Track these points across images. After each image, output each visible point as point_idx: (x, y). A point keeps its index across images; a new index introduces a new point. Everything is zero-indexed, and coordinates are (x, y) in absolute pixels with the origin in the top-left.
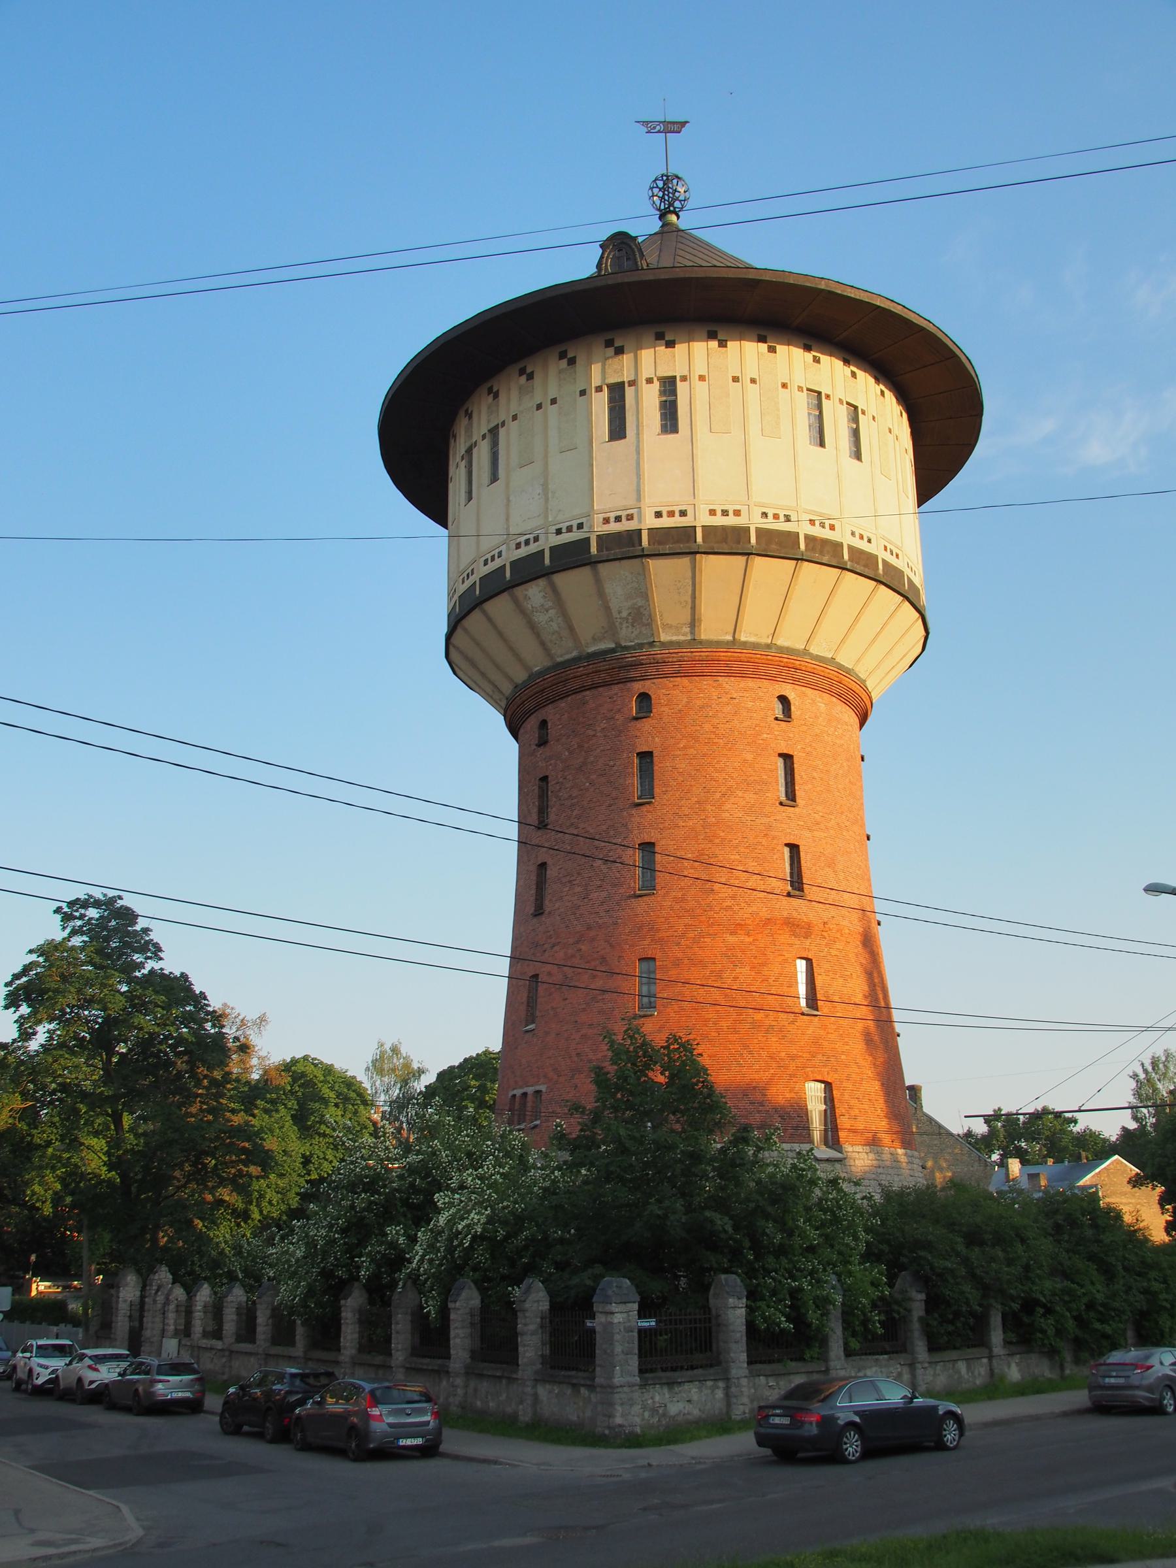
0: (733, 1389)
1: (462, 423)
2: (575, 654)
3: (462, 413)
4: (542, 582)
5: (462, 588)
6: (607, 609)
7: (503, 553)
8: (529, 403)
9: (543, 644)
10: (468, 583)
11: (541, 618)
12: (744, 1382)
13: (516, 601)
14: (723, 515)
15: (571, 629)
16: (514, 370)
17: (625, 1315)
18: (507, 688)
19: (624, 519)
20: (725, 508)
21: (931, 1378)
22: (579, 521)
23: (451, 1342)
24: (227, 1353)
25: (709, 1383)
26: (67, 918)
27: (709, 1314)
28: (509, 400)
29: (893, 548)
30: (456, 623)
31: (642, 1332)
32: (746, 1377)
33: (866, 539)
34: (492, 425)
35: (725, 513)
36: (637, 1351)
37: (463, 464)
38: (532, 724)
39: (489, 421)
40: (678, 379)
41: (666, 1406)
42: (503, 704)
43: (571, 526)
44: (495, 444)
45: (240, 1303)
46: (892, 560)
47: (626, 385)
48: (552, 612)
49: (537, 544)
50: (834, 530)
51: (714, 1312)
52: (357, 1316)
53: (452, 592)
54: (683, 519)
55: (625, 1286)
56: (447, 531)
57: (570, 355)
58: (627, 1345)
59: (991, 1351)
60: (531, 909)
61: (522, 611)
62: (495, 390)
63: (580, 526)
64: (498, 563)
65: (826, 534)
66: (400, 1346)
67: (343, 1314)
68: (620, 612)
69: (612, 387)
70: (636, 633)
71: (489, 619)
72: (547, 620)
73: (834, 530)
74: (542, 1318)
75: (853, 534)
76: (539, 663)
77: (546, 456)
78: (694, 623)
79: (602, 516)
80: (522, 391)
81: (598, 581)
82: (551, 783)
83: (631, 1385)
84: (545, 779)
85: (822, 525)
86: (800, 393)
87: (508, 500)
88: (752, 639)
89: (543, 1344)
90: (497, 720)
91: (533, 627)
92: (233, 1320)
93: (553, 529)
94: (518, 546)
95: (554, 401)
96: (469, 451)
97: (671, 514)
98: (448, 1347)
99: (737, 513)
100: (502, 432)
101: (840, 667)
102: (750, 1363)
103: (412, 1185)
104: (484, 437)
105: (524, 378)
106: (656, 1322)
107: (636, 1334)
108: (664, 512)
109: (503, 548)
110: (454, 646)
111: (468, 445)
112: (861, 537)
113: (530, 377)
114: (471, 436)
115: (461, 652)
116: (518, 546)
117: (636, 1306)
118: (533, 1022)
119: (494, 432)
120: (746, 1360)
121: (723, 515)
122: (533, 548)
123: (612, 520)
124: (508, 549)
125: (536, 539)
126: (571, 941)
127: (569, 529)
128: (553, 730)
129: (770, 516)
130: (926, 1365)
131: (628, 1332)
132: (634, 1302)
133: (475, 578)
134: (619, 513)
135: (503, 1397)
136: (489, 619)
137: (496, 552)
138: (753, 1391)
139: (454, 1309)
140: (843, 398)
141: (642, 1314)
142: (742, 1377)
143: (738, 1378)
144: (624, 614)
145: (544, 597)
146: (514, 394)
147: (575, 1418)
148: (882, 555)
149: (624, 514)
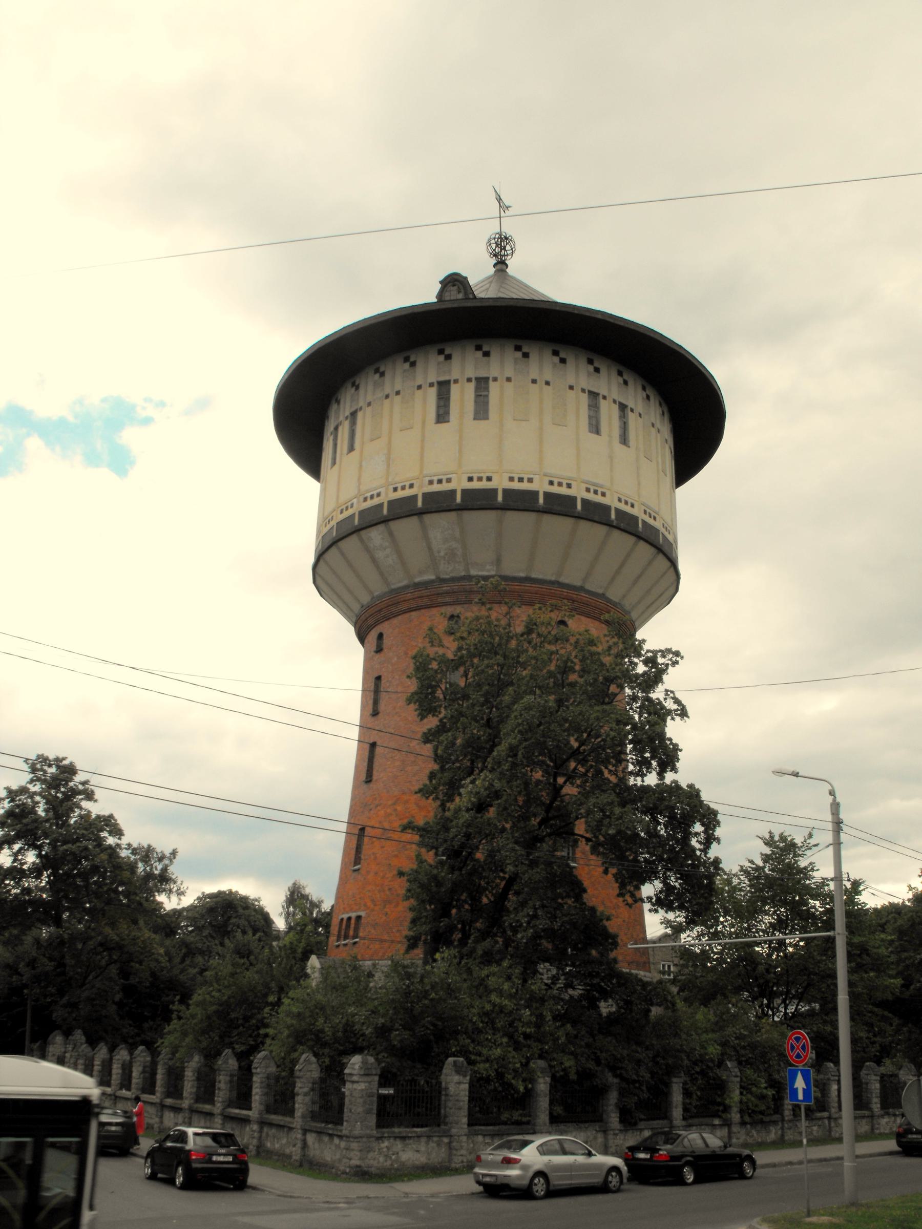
0: (454, 1144)
1: (334, 407)
2: (405, 583)
3: (333, 401)
4: (381, 527)
5: (325, 530)
6: (430, 548)
7: (355, 505)
8: (380, 394)
9: (381, 574)
10: (329, 527)
11: (380, 555)
12: (464, 1139)
13: (362, 540)
14: (519, 481)
15: (403, 563)
16: (371, 371)
17: (367, 1084)
18: (356, 608)
19: (444, 481)
20: (521, 476)
21: (621, 1142)
22: (411, 482)
23: (253, 1098)
24: (113, 1097)
25: (435, 1139)
26: (34, 769)
27: (192, 1111)
28: (366, 391)
29: (651, 512)
30: (320, 557)
31: (382, 1099)
32: (465, 1135)
33: (629, 504)
34: (353, 409)
35: (521, 480)
36: (375, 1111)
37: (331, 438)
38: (372, 636)
39: (351, 406)
40: (491, 379)
41: (398, 1153)
42: (354, 620)
43: (405, 486)
44: (353, 423)
45: (124, 1061)
46: (651, 521)
47: (452, 382)
48: (388, 551)
49: (379, 498)
50: (570, 487)
51: (443, 1085)
52: (196, 1074)
53: (324, 520)
54: (439, 485)
55: (370, 1062)
56: (308, 486)
57: (412, 359)
58: (367, 1106)
59: (671, 1122)
60: (363, 777)
61: (367, 549)
62: (357, 384)
63: (411, 486)
64: (350, 512)
65: (598, 499)
66: (220, 1099)
67: (186, 1073)
68: (439, 552)
69: (440, 384)
70: (450, 568)
71: (343, 554)
72: (386, 556)
73: (570, 487)
74: (313, 1083)
75: (551, 483)
76: (379, 588)
77: (390, 433)
78: (498, 561)
79: (428, 479)
80: (376, 384)
81: (424, 528)
82: (383, 681)
83: (369, 1137)
84: (379, 678)
85: (596, 492)
86: (583, 394)
87: (361, 466)
88: (540, 577)
89: (313, 1103)
90: (348, 630)
91: (374, 561)
92: (118, 1074)
93: (506, 476)
94: (365, 499)
95: (398, 393)
96: (336, 429)
97: (480, 479)
98: (251, 1102)
99: (530, 480)
100: (360, 415)
101: (609, 601)
102: (470, 1125)
103: (739, 956)
104: (347, 418)
105: (377, 375)
106: (395, 1090)
107: (375, 1099)
108: (475, 476)
109: (355, 501)
110: (320, 576)
111: (336, 424)
112: (626, 503)
113: (382, 374)
114: (338, 417)
115: (323, 579)
116: (365, 499)
117: (377, 1078)
118: (359, 864)
119: (354, 414)
120: (467, 1122)
121: (519, 481)
122: (376, 501)
123: (435, 482)
124: (358, 502)
125: (379, 495)
126: (390, 803)
127: (403, 488)
128: (386, 642)
129: (556, 484)
130: (617, 1132)
131: (369, 1096)
132: (376, 1075)
133: (333, 523)
134: (440, 477)
135: (284, 1141)
136: (343, 554)
137: (349, 504)
138: (472, 1145)
139: (256, 1073)
140: (584, 387)
141: (382, 1085)
142: (462, 1135)
143: (459, 1136)
144: (442, 554)
145: (383, 539)
146: (370, 388)
147: (329, 1159)
148: (642, 517)
149: (444, 478)
